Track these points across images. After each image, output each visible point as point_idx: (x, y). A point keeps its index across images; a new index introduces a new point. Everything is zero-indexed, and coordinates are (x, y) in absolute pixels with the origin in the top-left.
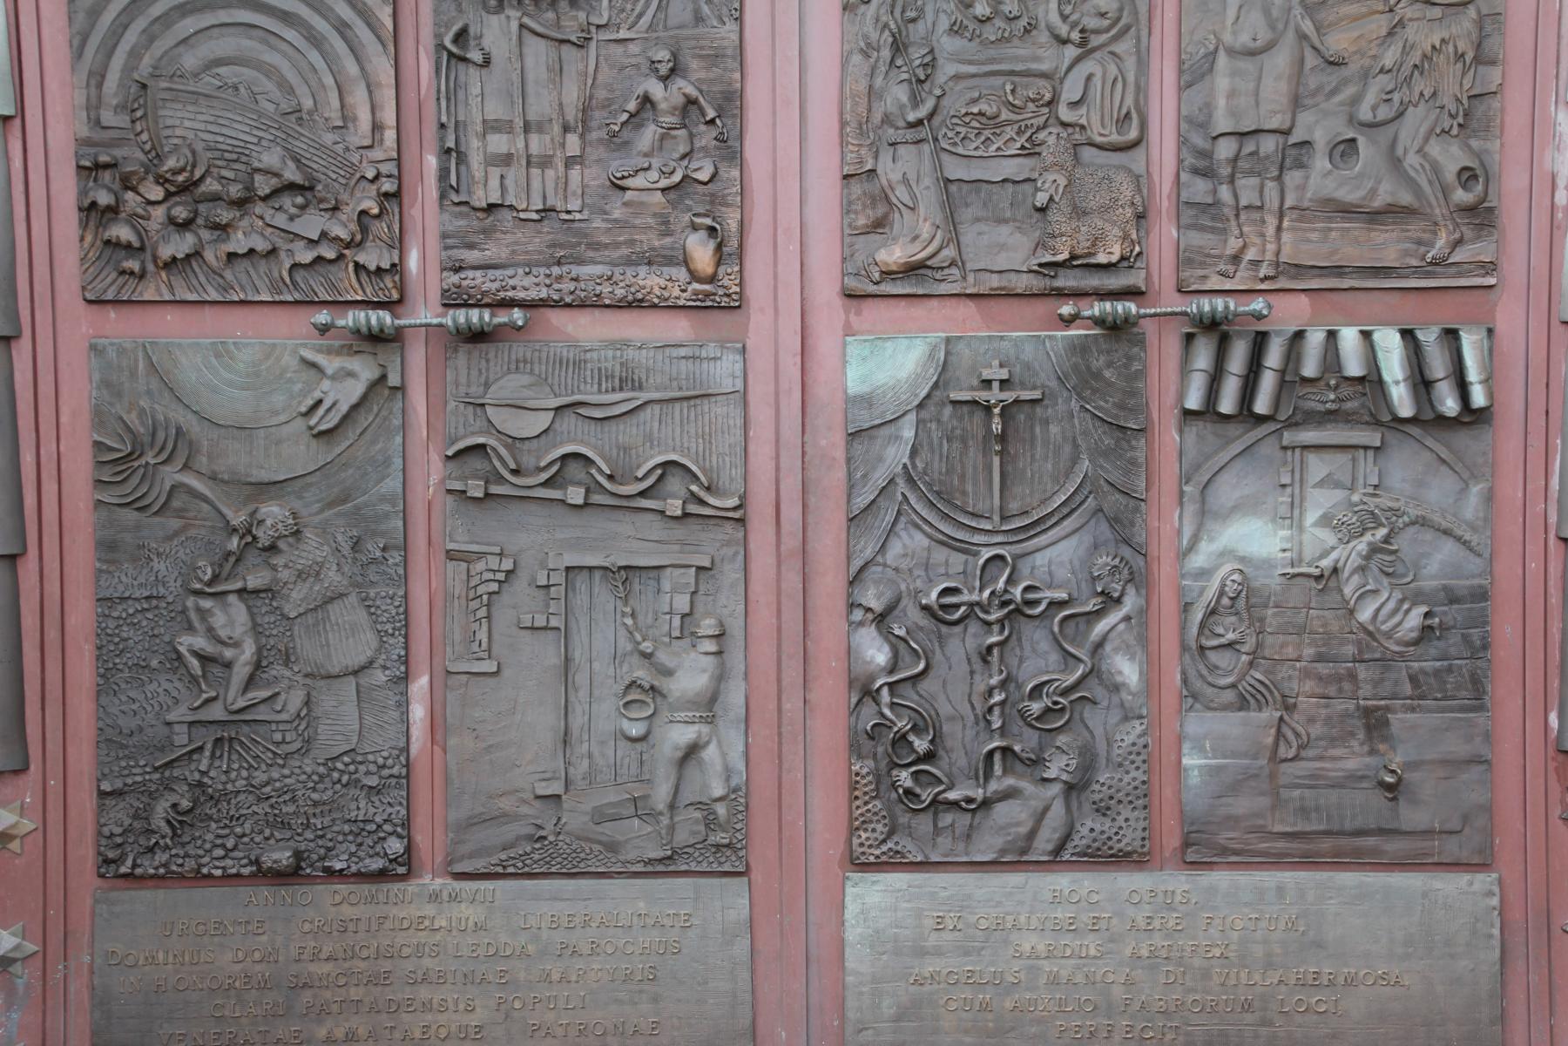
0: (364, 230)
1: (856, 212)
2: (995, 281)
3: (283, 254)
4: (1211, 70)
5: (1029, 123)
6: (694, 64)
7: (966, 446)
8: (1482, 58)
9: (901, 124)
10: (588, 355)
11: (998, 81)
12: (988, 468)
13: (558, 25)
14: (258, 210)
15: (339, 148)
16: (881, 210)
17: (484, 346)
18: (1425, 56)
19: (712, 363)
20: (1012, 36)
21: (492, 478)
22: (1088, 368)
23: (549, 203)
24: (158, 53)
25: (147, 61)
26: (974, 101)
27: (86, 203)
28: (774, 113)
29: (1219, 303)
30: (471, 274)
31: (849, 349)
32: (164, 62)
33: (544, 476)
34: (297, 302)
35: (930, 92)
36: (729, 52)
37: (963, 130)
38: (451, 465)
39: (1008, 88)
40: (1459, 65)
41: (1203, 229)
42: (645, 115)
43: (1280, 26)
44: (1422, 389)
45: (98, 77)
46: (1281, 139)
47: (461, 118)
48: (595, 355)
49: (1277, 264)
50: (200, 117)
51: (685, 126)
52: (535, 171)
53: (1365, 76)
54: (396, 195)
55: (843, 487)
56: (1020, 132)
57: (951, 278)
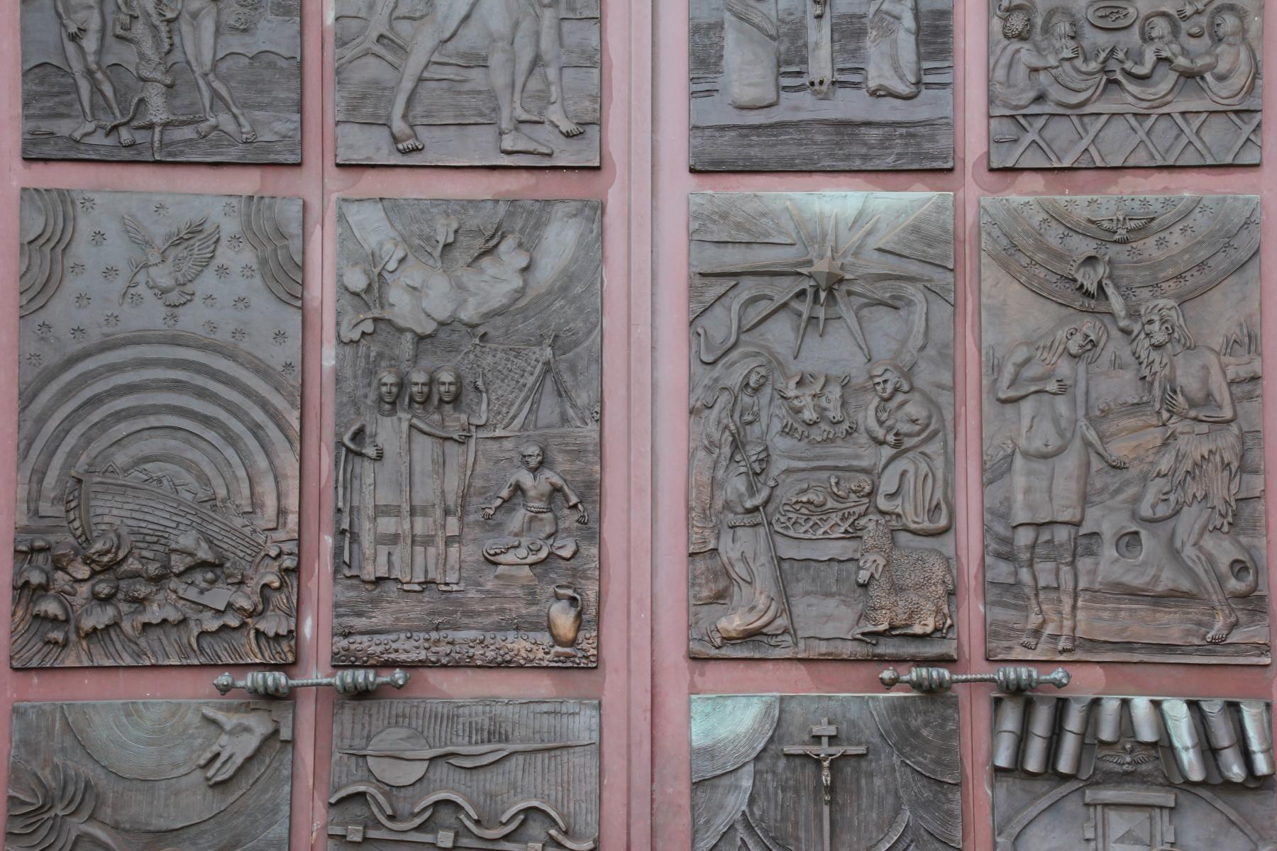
0: (266, 600)
1: (700, 585)
2: (823, 648)
3: (192, 624)
4: (1009, 469)
5: (851, 511)
6: (560, 458)
7: (799, 797)
8: (1245, 468)
9: (740, 510)
10: (461, 710)
11: (825, 475)
12: (819, 816)
13: (443, 427)
14: (172, 585)
15: (247, 531)
16: (722, 584)
17: (367, 703)
18: (1195, 464)
19: (571, 718)
20: (836, 437)
21: (370, 823)
22: (908, 727)
23: (430, 576)
24: (94, 453)
25: (84, 459)
26: (804, 491)
27: (20, 582)
28: (629, 499)
29: (1024, 672)
30: (358, 638)
31: (694, 706)
32: (99, 458)
33: (418, 821)
34: (202, 666)
35: (765, 484)
36: (591, 448)
37: (794, 516)
38: (333, 811)
39: (833, 481)
40: (1226, 473)
41: (1006, 605)
42: (515, 501)
43: (1068, 435)
44: (1209, 754)
45: (40, 474)
46: (1073, 530)
47: (355, 504)
48: (467, 710)
49: (1074, 639)
50: (126, 506)
51: (551, 510)
52: (419, 549)
53: (1144, 479)
54: (296, 571)
55: (689, 833)
56: (843, 519)
57: (784, 644)
